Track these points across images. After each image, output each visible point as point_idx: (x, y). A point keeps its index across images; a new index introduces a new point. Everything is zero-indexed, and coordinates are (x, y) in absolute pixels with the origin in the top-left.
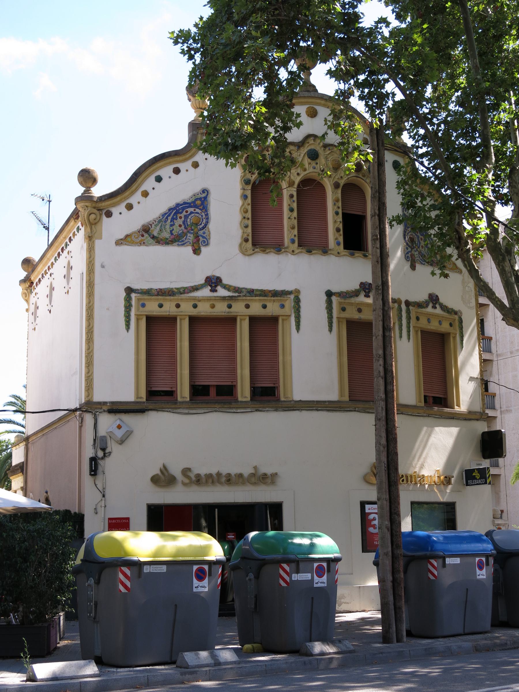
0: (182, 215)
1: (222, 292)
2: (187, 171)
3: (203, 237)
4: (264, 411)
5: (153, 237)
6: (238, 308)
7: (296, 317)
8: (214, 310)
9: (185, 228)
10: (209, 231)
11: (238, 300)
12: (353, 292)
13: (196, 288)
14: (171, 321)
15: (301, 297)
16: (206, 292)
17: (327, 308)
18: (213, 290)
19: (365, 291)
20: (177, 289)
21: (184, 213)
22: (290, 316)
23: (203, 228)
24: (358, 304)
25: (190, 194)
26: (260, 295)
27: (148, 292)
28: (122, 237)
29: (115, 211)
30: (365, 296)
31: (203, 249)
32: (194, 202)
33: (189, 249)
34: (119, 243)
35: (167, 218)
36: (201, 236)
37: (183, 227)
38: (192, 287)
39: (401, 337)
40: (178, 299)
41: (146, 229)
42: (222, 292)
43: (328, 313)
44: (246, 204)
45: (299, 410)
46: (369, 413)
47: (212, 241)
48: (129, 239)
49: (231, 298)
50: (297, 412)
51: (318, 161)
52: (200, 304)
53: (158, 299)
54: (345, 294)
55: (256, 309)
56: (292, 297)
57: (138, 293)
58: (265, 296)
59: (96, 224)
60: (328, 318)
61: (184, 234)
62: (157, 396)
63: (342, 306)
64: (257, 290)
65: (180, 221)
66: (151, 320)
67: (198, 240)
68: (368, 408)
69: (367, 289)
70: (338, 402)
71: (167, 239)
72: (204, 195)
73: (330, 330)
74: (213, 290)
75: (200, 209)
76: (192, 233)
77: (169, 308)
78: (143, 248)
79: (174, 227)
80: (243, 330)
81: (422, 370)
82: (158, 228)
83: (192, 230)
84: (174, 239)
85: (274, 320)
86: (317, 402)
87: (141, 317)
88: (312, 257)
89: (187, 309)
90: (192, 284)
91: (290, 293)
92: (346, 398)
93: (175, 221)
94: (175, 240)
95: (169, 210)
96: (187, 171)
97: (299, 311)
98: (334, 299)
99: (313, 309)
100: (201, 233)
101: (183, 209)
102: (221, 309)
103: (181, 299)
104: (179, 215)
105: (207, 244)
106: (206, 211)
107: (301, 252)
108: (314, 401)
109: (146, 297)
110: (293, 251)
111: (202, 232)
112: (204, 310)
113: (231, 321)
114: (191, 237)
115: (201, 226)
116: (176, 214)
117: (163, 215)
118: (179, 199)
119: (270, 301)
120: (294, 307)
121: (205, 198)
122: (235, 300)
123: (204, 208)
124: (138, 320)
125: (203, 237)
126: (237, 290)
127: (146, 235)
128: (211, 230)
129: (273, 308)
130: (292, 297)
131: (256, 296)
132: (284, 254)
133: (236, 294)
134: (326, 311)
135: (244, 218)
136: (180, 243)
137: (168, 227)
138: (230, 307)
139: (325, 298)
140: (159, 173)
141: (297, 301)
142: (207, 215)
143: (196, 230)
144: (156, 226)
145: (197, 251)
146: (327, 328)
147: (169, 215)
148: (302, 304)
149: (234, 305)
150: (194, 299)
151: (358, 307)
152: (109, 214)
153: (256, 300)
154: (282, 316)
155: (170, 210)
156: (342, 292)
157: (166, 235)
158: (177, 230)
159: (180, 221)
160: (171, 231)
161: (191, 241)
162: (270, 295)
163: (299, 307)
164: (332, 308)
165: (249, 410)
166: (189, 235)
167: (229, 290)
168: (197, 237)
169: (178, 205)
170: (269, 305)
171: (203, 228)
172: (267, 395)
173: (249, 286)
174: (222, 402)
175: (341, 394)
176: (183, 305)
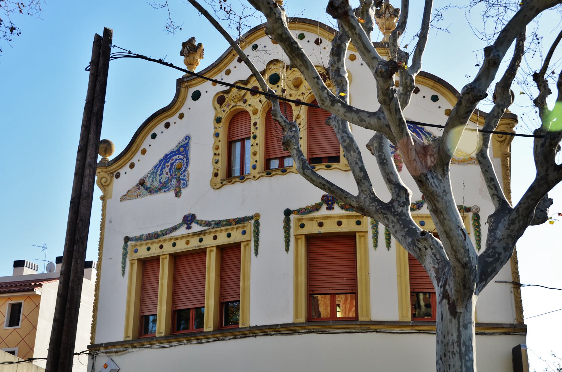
0: (169, 164)
1: (196, 228)
2: (175, 123)
3: (184, 180)
4: (223, 340)
5: (147, 189)
6: (208, 241)
7: (255, 241)
8: (189, 246)
9: (171, 175)
10: (188, 174)
11: (207, 233)
12: (313, 206)
13: (175, 228)
14: (156, 260)
15: (260, 221)
16: (183, 231)
17: (284, 227)
18: (189, 228)
19: (327, 204)
20: (161, 231)
21: (171, 162)
22: (250, 240)
23: (184, 171)
24: (318, 218)
25: (177, 143)
26: (226, 225)
27: (140, 238)
28: (125, 193)
29: (122, 171)
30: (328, 209)
31: (183, 191)
32: (178, 150)
33: (172, 193)
34: (123, 199)
35: (158, 169)
36: (182, 179)
37: (169, 174)
38: (172, 228)
39: (376, 246)
40: (160, 241)
41: (142, 183)
42: (196, 228)
43: (285, 232)
44: (217, 141)
45: (253, 336)
46: (329, 333)
47: (190, 183)
48: (129, 194)
49: (202, 233)
50: (252, 338)
51: (278, 84)
52: (178, 242)
53: (146, 244)
54: (304, 210)
55: (223, 239)
56: (253, 222)
57: (133, 241)
58: (230, 225)
59: (108, 185)
60: (285, 237)
61: (169, 180)
62: (143, 332)
63: (300, 223)
64: (223, 221)
65: (167, 170)
66: (310, 239)
67: (180, 184)
68: (327, 329)
69: (330, 201)
70: (293, 324)
71: (156, 188)
72: (186, 142)
73: (287, 249)
74: (189, 228)
75: (183, 155)
76: (175, 178)
77: (155, 251)
78: (140, 200)
79: (162, 176)
80: (212, 260)
81: (206, 286)
82: (151, 179)
83: (176, 175)
84: (162, 186)
85: (237, 246)
86: (270, 326)
87: (299, 237)
88: (272, 178)
89: (168, 249)
90: (173, 225)
91: (250, 218)
92: (302, 319)
93: (163, 170)
94: (163, 187)
95: (160, 161)
96: (308, 41)
97: (258, 235)
98: (292, 217)
99: (272, 231)
100: (182, 176)
101: (170, 158)
102: (194, 244)
103: (164, 241)
104: (167, 164)
105: (186, 185)
106: (187, 156)
107: (262, 176)
108: (267, 326)
109: (138, 243)
110: (254, 177)
111: (182, 175)
112: (181, 247)
113: (201, 253)
114: (174, 181)
115: (182, 170)
116: (164, 164)
117: (155, 167)
118: (167, 151)
119: (233, 229)
120: (254, 231)
121: (187, 144)
122: (205, 233)
123: (185, 153)
124: (132, 264)
125: (184, 180)
126: (208, 224)
127: (142, 188)
128: (190, 172)
129: (237, 236)
130: (253, 222)
131: (223, 226)
132: (248, 180)
133: (206, 228)
134: (283, 230)
135: (215, 154)
136: (166, 190)
137: (158, 176)
138: (201, 240)
139: (283, 217)
140: (306, 33)
141: (257, 224)
142: (187, 159)
143: (178, 175)
144: (149, 178)
145: (178, 194)
146: (284, 247)
147: (159, 167)
148: (261, 228)
149: (204, 238)
150: (173, 239)
151: (319, 221)
152: (118, 176)
153: (221, 231)
154: (243, 242)
155: (161, 161)
156: (301, 209)
157: (156, 184)
158: (164, 177)
159: (167, 170)
160: (160, 180)
161: (174, 186)
162: (234, 223)
163: (258, 230)
164: (290, 226)
165: (211, 340)
166: (173, 180)
167: (201, 225)
168: (179, 181)
169: (166, 155)
170: (233, 233)
171: (184, 171)
172: (229, 322)
173: (217, 218)
174: (188, 335)
175: (297, 315)
176: (166, 245)
